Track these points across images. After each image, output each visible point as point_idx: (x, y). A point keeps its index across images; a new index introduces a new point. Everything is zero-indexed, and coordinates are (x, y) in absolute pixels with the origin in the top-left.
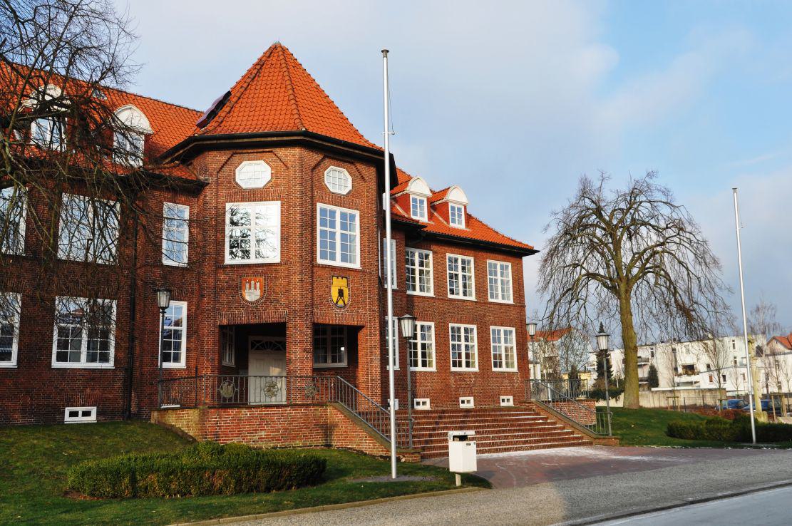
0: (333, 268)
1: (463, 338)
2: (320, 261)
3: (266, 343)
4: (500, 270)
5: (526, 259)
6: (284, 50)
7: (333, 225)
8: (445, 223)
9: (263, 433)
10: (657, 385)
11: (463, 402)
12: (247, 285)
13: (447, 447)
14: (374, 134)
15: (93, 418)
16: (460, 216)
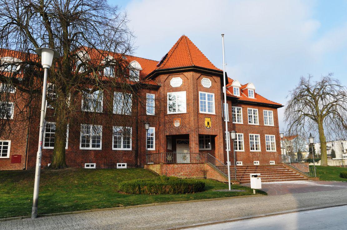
0: (205, 114)
1: (254, 139)
2: (200, 112)
3: (182, 141)
4: (268, 114)
5: (278, 109)
6: (186, 37)
7: (205, 99)
8: (246, 96)
9: (182, 173)
10: (335, 157)
11: (120, 165)
12: (175, 121)
13: (250, 180)
14: (219, 66)
15: (125, 167)
16: (252, 94)
